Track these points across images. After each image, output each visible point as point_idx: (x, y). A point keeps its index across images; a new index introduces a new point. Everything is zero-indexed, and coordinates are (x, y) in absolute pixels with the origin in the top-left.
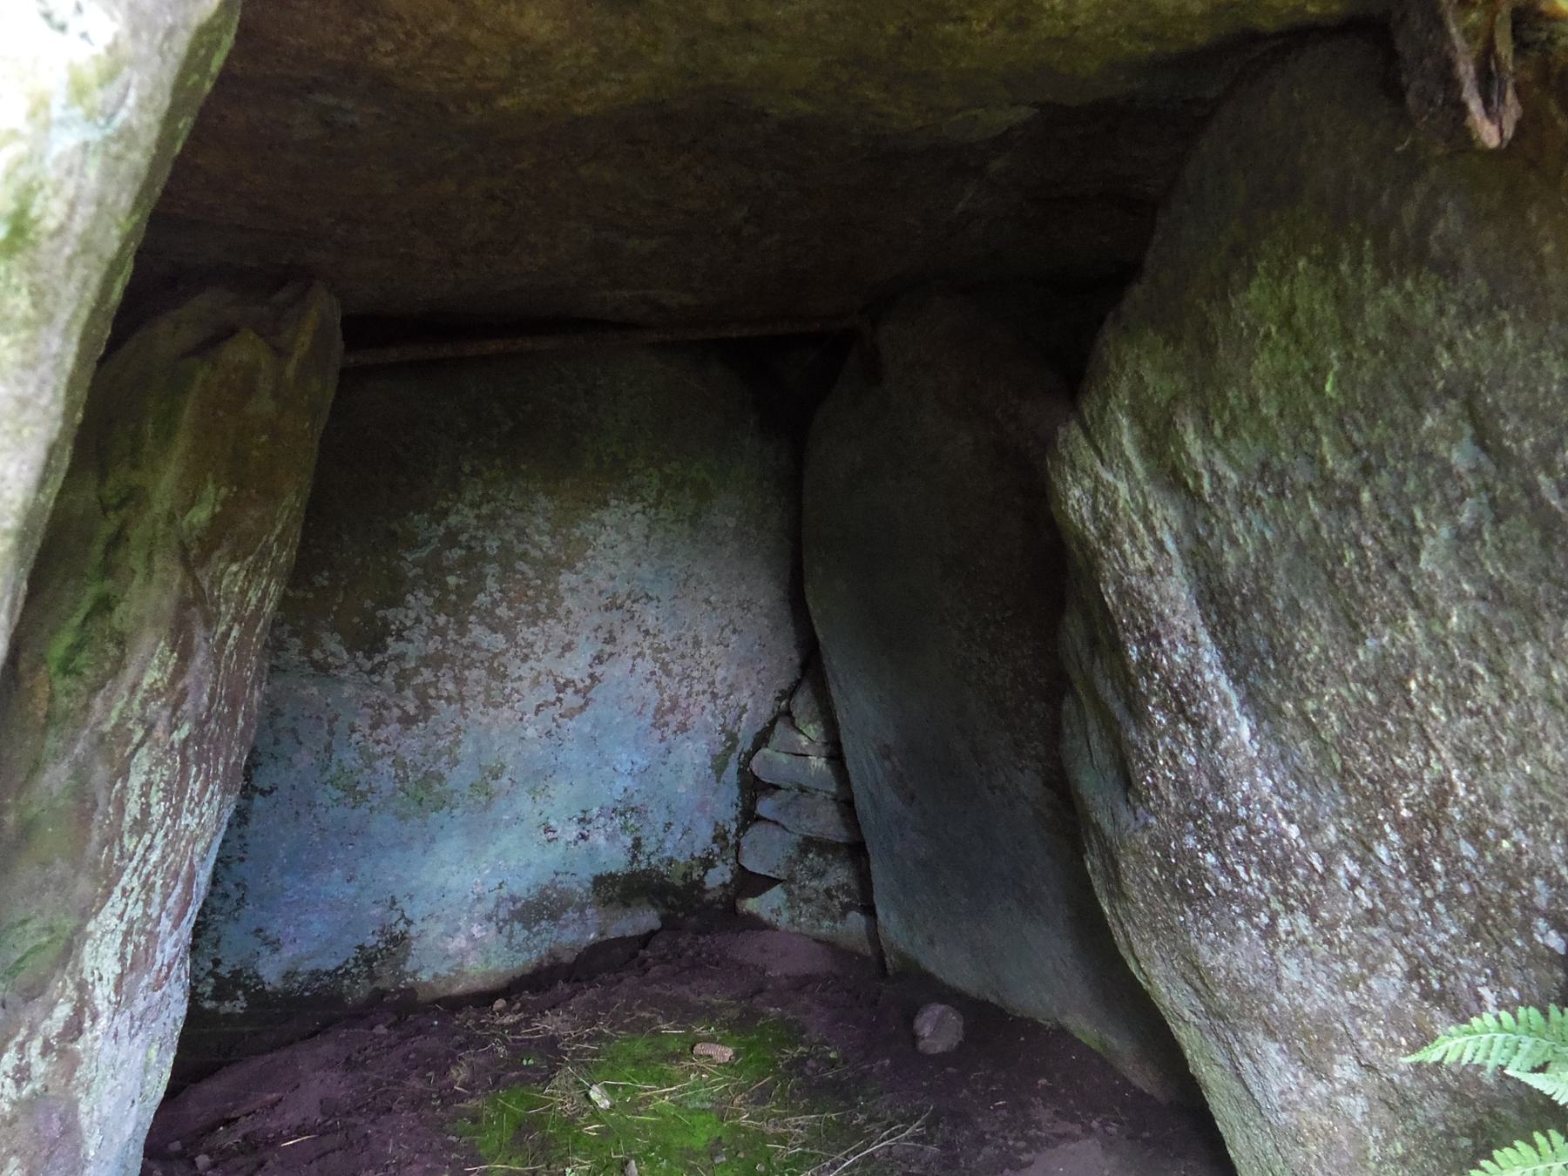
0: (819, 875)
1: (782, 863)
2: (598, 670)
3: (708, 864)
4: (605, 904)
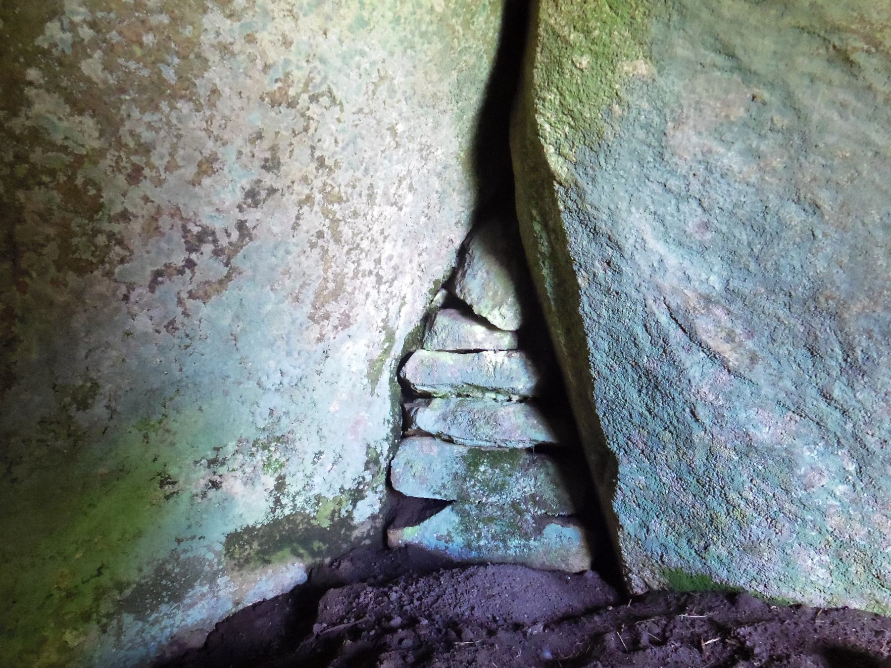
0: (498, 489)
1: (447, 480)
2: (252, 216)
3: (357, 495)
4: (240, 566)
